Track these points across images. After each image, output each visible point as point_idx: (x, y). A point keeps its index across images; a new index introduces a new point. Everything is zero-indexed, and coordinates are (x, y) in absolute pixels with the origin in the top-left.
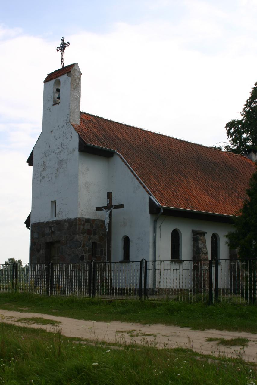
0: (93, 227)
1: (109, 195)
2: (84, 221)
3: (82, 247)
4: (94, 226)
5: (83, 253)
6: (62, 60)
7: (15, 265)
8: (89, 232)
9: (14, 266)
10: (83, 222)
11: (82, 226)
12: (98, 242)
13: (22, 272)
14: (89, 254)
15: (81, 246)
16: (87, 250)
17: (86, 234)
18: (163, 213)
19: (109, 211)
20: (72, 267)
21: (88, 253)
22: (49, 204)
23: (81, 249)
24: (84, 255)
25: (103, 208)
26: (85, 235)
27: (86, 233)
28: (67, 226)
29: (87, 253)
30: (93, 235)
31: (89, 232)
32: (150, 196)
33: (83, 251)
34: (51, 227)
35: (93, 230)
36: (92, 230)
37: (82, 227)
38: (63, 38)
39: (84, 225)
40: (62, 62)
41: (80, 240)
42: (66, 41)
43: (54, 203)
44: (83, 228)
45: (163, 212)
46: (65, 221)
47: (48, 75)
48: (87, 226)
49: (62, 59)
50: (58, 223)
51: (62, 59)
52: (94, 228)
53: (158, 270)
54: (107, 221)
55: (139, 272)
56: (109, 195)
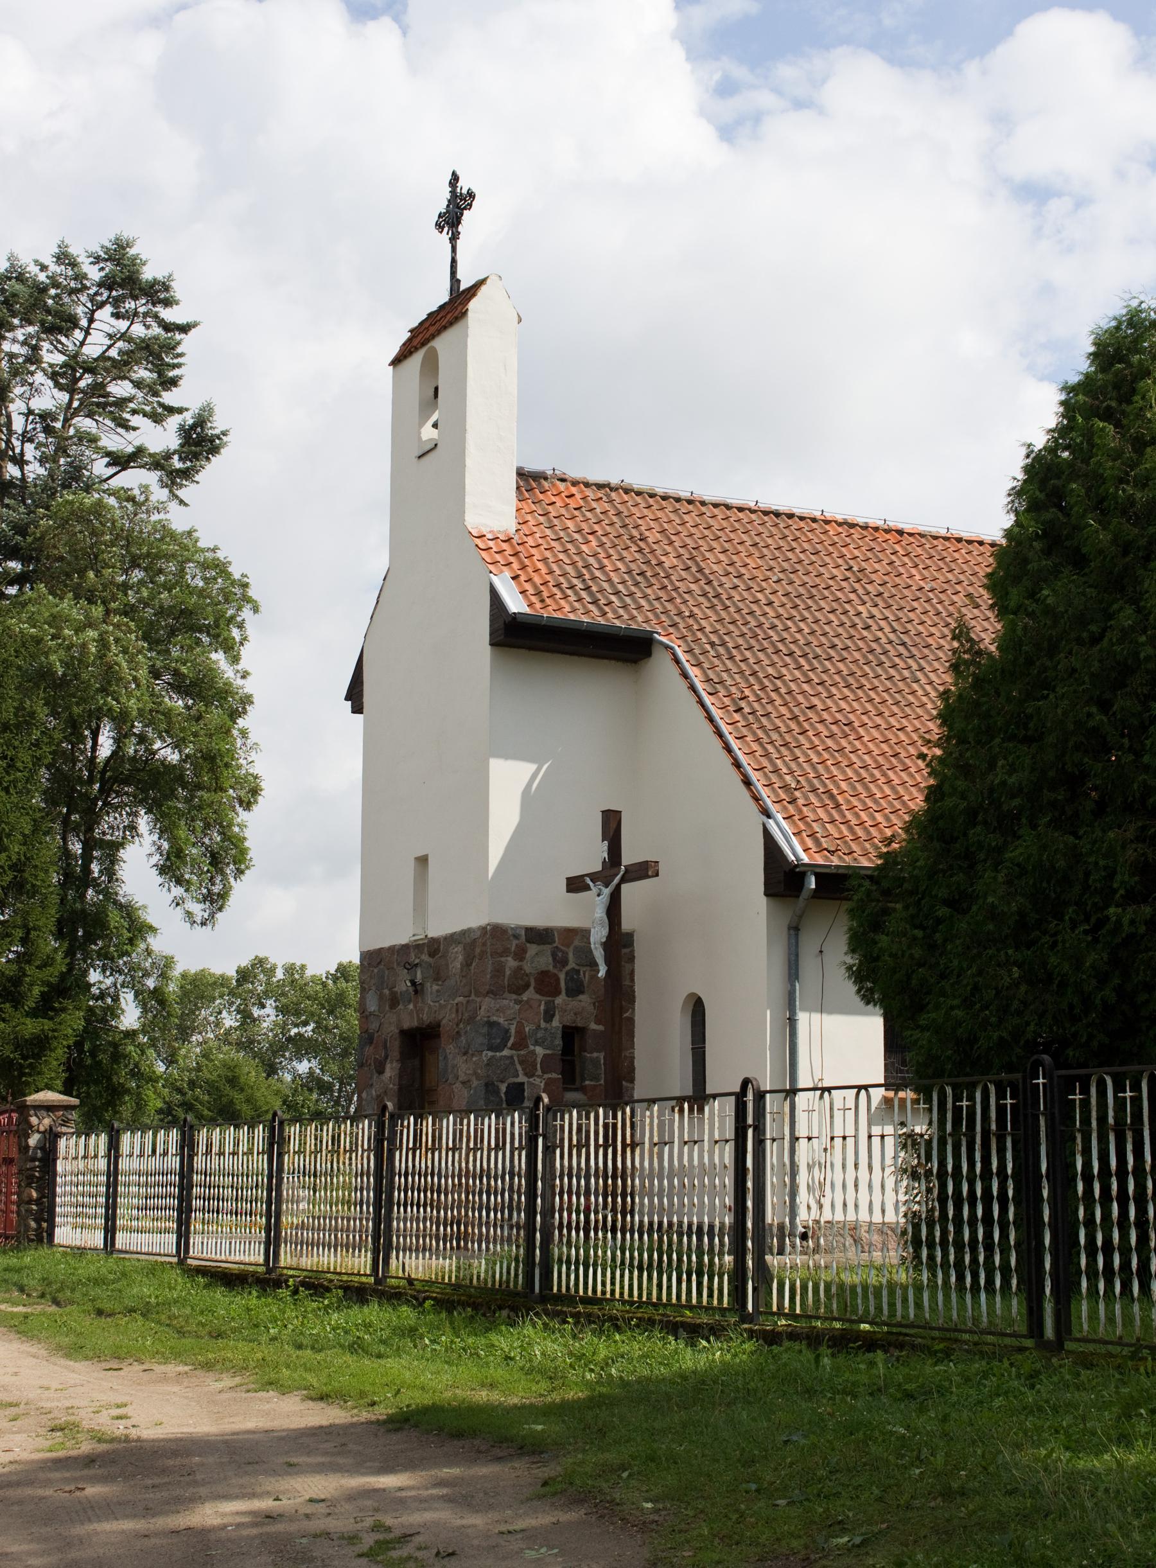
0: (564, 962)
1: (612, 825)
2: (523, 938)
3: (511, 1049)
4: (571, 956)
5: (517, 1076)
6: (452, 267)
7: (750, 1096)
8: (546, 984)
9: (745, 1103)
10: (515, 942)
11: (509, 959)
12: (593, 1026)
13: (366, 1154)
14: (546, 1076)
15: (509, 1044)
16: (539, 1060)
17: (529, 994)
18: (815, 890)
19: (607, 892)
20: (998, 1106)
21: (544, 1072)
22: (412, 864)
23: (512, 1057)
24: (523, 1084)
25: (588, 880)
26: (525, 997)
27: (531, 989)
28: (457, 958)
29: (539, 1072)
30: (567, 995)
31: (546, 984)
32: (764, 818)
33: (519, 1068)
34: (411, 967)
35: (567, 974)
36: (562, 976)
37: (511, 963)
38: (454, 174)
39: (520, 954)
40: (453, 272)
41: (501, 1020)
42: (464, 185)
43: (423, 861)
44: (520, 968)
45: (813, 886)
46: (451, 939)
47: (411, 331)
48: (538, 959)
49: (454, 261)
50: (434, 947)
51: (454, 261)
52: (571, 965)
53: (844, 1138)
54: (599, 934)
55: (729, 1150)
56: (612, 825)
